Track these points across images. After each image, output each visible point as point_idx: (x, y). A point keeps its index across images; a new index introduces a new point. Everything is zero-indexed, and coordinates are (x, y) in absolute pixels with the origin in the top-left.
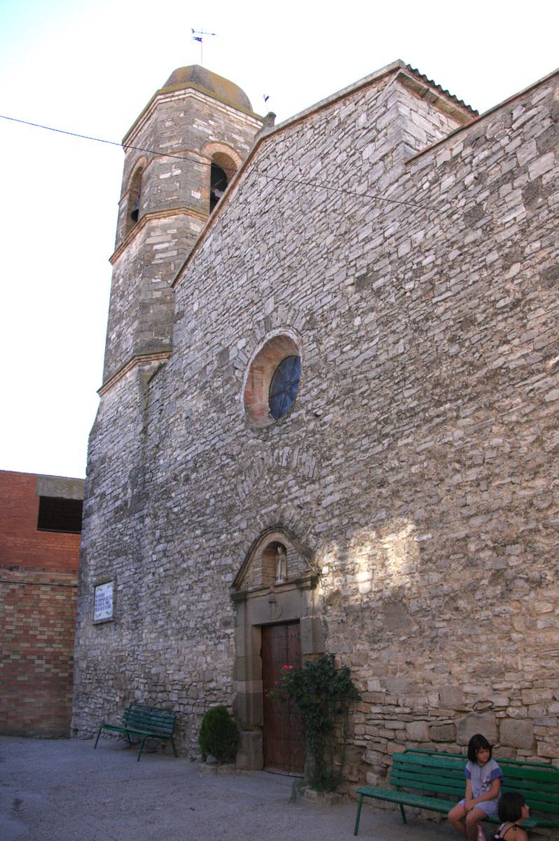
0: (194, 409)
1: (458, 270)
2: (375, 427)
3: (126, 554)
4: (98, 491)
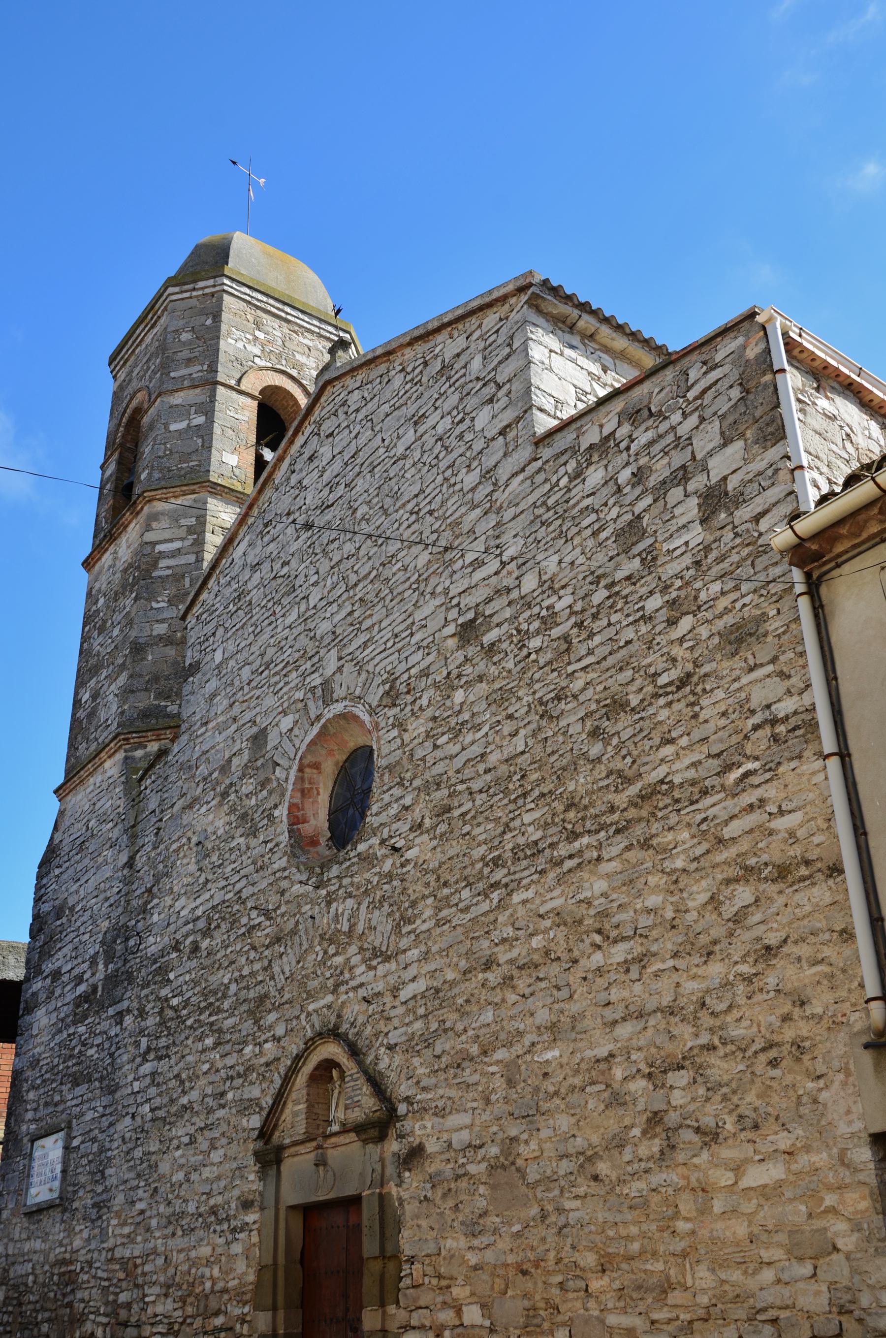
0: (210, 829)
1: (605, 622)
2: (481, 871)
3: (90, 1081)
4: (48, 967)
